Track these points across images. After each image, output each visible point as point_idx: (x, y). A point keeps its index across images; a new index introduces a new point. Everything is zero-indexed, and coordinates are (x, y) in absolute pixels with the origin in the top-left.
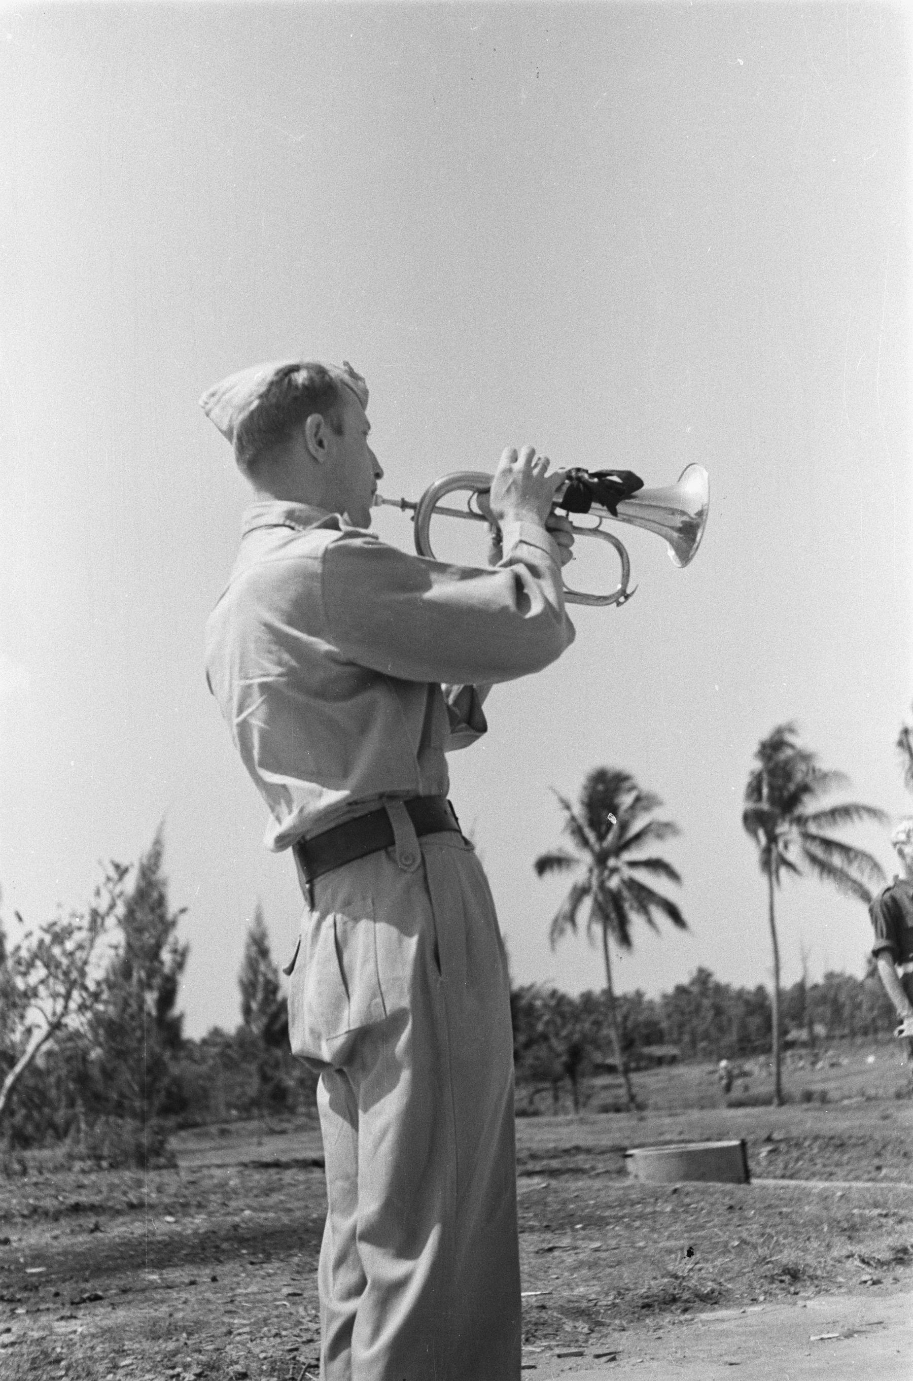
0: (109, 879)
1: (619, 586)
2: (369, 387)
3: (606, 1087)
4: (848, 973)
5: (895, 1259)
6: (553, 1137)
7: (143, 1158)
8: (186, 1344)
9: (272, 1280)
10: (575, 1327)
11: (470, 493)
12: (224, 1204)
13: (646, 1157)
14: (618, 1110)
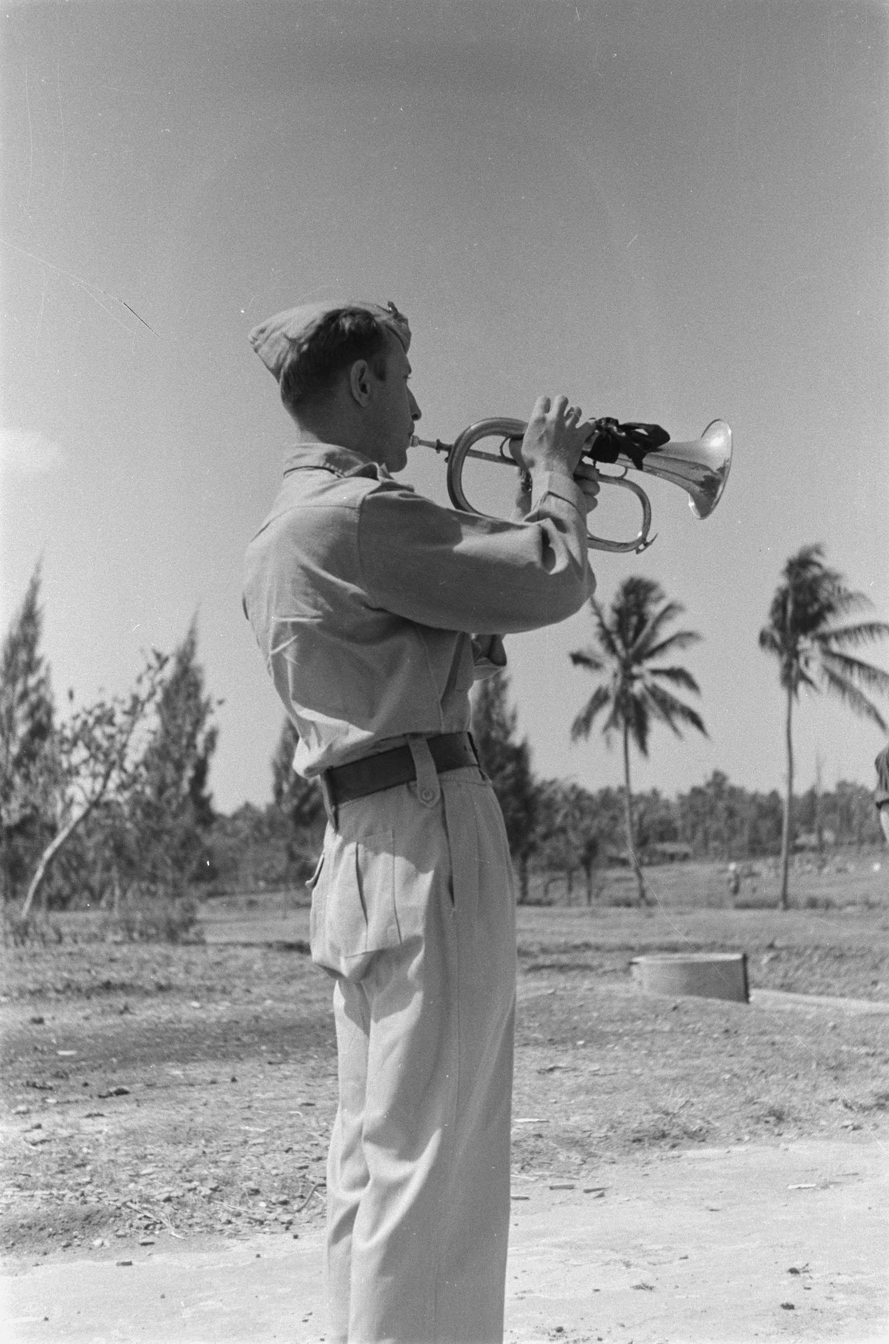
0: (150, 667)
1: (640, 534)
2: (411, 329)
3: (618, 880)
4: (860, 783)
5: (876, 1105)
6: (565, 929)
7: (173, 933)
8: (204, 1152)
9: (289, 1085)
10: (568, 1157)
11: (503, 438)
12: (248, 991)
13: (650, 966)
14: (628, 905)
